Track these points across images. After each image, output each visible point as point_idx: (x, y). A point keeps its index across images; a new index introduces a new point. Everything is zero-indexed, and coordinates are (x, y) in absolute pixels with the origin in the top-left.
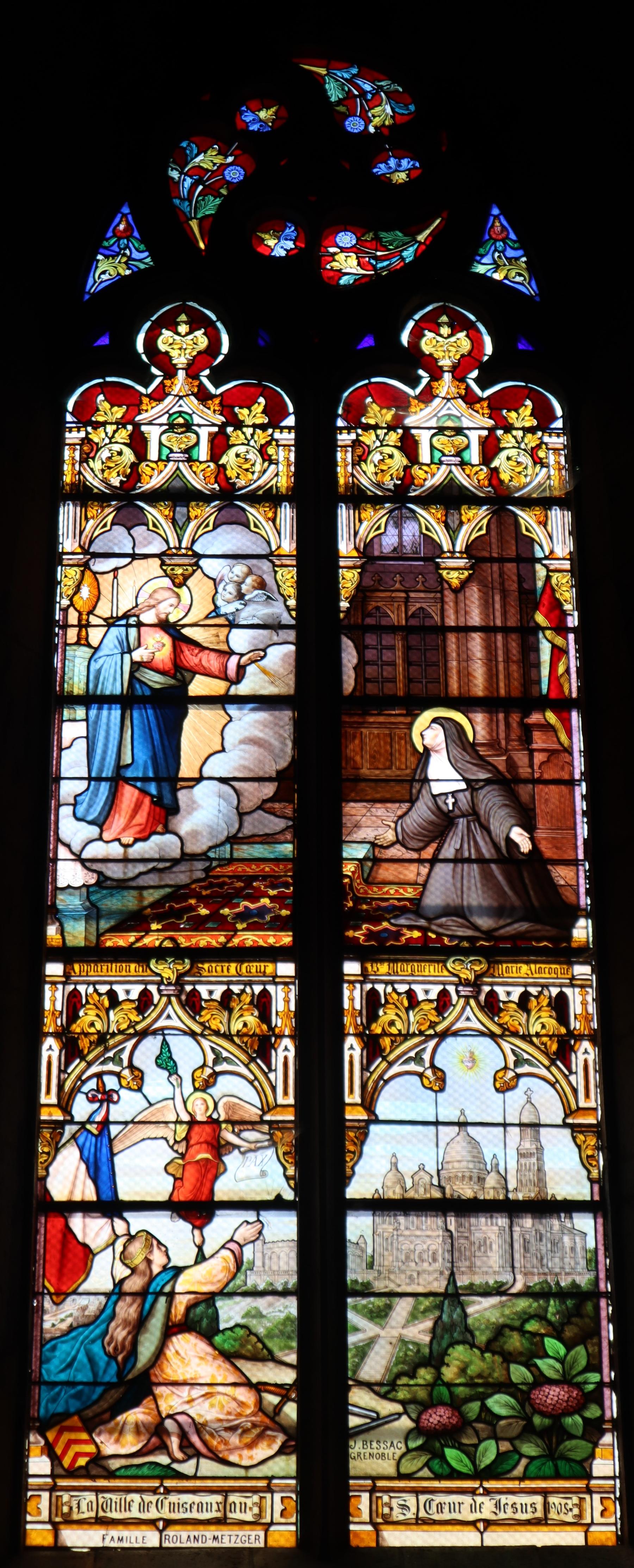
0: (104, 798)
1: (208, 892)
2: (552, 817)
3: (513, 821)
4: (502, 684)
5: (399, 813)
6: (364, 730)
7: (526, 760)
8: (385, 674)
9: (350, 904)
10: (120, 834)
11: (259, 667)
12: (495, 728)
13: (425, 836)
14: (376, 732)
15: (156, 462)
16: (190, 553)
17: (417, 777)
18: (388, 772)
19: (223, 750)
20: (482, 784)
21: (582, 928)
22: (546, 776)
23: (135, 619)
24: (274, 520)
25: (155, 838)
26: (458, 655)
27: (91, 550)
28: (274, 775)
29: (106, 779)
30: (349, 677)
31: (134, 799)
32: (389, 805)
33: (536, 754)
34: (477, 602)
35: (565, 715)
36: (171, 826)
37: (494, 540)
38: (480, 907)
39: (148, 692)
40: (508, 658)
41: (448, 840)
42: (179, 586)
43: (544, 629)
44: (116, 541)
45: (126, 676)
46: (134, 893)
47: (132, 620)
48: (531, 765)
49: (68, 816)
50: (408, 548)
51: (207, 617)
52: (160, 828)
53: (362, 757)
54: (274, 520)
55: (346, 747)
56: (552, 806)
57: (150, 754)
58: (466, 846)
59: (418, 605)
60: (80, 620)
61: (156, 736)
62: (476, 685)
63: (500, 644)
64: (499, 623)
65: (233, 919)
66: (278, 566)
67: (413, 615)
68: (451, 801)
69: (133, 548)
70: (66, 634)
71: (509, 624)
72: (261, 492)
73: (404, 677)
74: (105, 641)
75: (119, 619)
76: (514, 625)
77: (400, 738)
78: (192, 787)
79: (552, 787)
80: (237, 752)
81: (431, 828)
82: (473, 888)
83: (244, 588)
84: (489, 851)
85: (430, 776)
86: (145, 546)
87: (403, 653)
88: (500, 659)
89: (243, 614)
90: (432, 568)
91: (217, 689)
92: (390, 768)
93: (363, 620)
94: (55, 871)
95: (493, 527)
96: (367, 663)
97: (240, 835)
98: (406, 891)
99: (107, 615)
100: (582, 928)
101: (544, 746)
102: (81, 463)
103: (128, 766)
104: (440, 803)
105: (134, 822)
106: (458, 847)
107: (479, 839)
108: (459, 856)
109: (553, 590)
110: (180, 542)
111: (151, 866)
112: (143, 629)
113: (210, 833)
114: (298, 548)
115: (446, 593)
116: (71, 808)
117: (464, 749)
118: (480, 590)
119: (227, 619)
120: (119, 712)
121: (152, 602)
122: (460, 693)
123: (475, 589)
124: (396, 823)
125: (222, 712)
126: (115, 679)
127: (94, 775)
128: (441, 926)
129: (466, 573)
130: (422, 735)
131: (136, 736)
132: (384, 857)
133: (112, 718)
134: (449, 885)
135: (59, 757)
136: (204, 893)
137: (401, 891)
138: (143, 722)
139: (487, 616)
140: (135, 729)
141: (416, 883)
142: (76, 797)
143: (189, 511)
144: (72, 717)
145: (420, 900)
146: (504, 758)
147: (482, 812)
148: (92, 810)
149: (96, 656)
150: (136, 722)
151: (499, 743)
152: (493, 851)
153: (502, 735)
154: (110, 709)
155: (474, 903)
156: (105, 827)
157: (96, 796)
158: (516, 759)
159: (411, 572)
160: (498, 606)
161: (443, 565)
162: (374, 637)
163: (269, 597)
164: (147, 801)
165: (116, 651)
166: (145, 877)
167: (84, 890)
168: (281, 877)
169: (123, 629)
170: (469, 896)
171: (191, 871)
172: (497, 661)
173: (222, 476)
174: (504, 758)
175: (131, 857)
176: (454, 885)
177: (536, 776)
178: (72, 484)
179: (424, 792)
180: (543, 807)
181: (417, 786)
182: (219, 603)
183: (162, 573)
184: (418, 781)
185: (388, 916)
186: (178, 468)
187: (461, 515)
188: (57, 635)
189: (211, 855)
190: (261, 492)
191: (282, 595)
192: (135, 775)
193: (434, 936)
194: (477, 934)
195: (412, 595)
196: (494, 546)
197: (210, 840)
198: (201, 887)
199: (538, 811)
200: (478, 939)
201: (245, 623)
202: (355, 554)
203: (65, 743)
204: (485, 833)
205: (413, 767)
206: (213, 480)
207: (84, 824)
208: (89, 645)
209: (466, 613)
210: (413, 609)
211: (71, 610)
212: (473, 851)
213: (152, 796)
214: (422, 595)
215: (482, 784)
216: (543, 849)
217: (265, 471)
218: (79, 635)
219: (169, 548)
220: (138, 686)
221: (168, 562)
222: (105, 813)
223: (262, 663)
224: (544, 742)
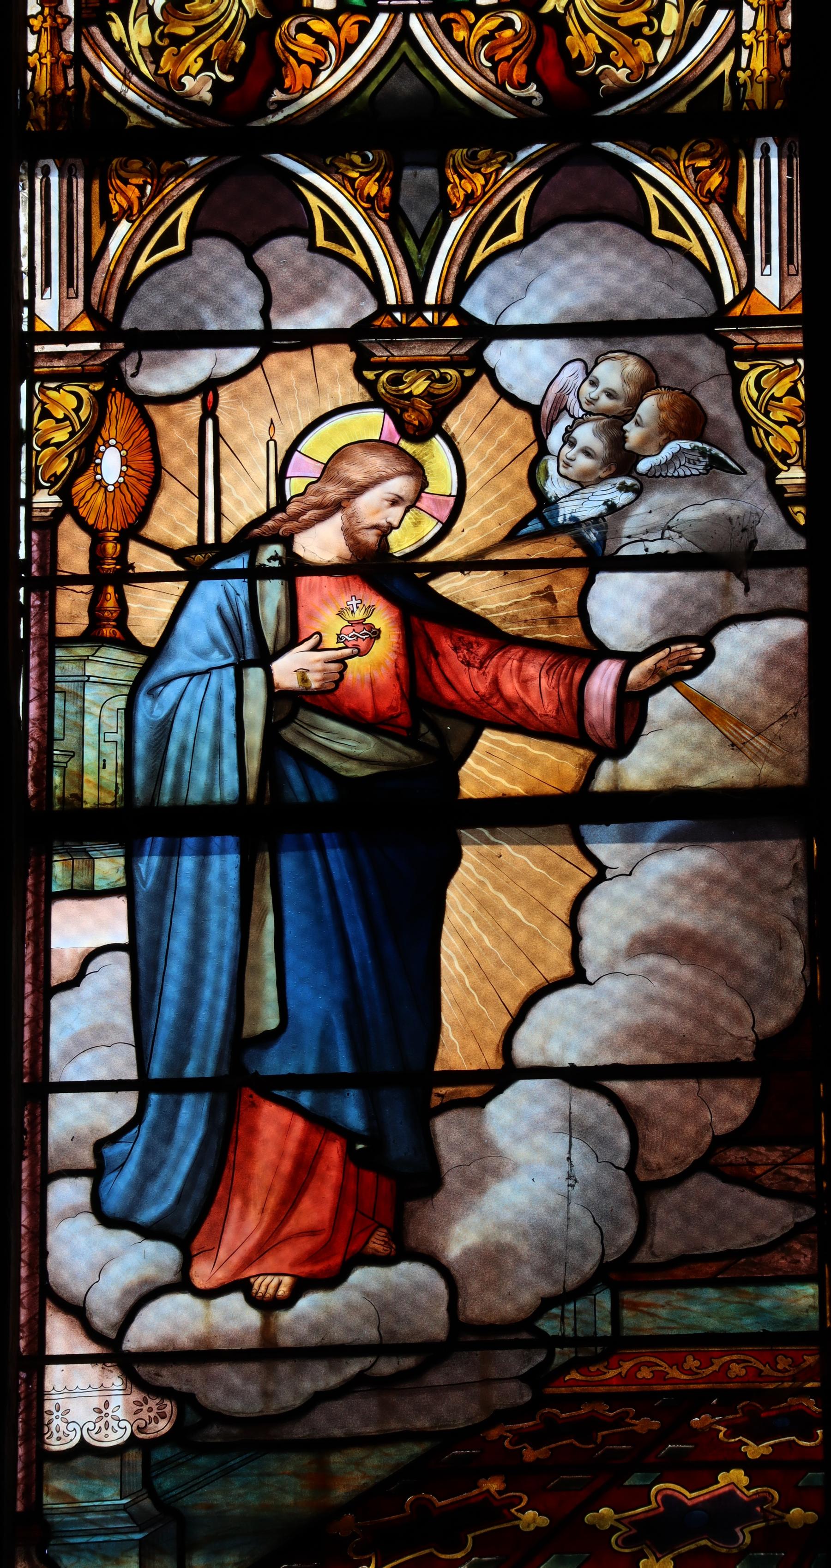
0: (193, 1147)
1: (543, 1452)
10: (248, 1262)
11: (690, 696)
15: (330, 16)
16: (452, 322)
19: (578, 977)
23: (276, 549)
24: (726, 201)
25: (360, 1276)
27: (127, 323)
28: (746, 1054)
29: (197, 1086)
31: (292, 1147)
36: (413, 1240)
39: (324, 791)
42: (421, 436)
44: (205, 287)
45: (254, 738)
46: (299, 1461)
47: (268, 554)
49: (76, 1212)
51: (513, 537)
52: (377, 1244)
54: (726, 201)
57: (338, 991)
60: (96, 556)
61: (356, 929)
65: (627, 1541)
66: (743, 356)
69: (265, 313)
70: (51, 607)
72: (681, 106)
74: (183, 624)
75: (225, 550)
78: (481, 1102)
80: (617, 987)
83: (634, 434)
86: (305, 301)
89: (630, 526)
91: (557, 770)
94: (39, 1394)
97: (643, 1257)
99: (186, 537)
102: (81, 23)
103: (270, 1038)
105: (292, 1226)
110: (419, 287)
111: (353, 1367)
112: (304, 583)
113: (545, 1249)
114: (806, 294)
116: (84, 1184)
119: (580, 542)
120: (233, 859)
121: (333, 492)
125: (571, 851)
126: (217, 751)
127: (156, 1071)
131: (290, 933)
133: (213, 878)
135: (43, 1018)
136: (529, 1455)
138: (311, 883)
140: (289, 911)
142: (99, 1146)
143: (444, 182)
144: (81, 880)
148: (154, 1188)
149: (154, 678)
150: (288, 889)
154: (204, 852)
156: (196, 1244)
157: (168, 1139)
163: (715, 463)
164: (334, 1152)
165: (217, 658)
166: (338, 1406)
167: (134, 1456)
168: (779, 1395)
169: (239, 586)
171: (486, 1381)
173: (550, 52)
175: (286, 1340)
178: (57, 98)
182: (555, 487)
183: (358, 394)
186: (406, 33)
188: (25, 611)
189: (549, 1326)
190: (681, 106)
191: (761, 453)
192: (289, 1068)
197: (543, 1272)
198: (520, 1437)
201: (637, 550)
203: (61, 970)
206: (519, 72)
207: (128, 1236)
208: (130, 643)
211: (67, 524)
213: (349, 1136)
217: (696, 34)
218: (95, 608)
219: (383, 308)
220: (292, 772)
221: (380, 354)
222: (197, 1196)
223: (694, 683)
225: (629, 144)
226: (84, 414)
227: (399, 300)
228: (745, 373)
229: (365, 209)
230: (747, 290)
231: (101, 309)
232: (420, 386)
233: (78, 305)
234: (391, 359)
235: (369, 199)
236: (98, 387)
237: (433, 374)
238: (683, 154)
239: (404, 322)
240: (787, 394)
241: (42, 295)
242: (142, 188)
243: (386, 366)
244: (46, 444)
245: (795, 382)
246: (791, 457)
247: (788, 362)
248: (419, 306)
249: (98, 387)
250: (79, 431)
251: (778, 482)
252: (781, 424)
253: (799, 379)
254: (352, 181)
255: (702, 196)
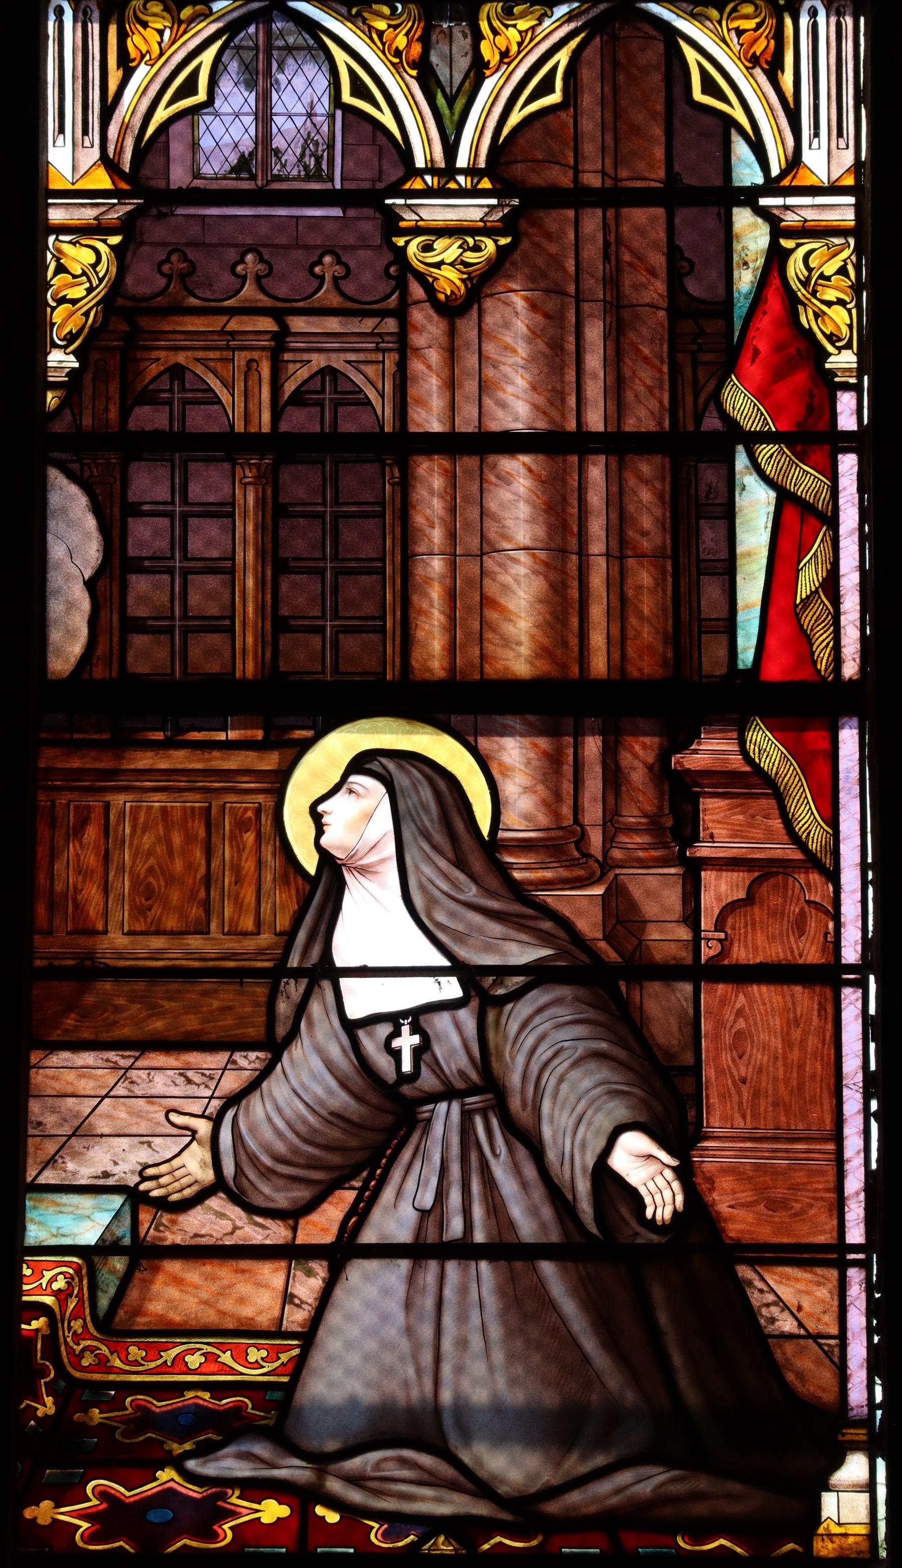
2: (756, 1094)
3: (620, 1111)
4: (598, 639)
5: (231, 1083)
6: (119, 800)
7: (673, 897)
8: (194, 599)
9: (48, 1406)
12: (567, 787)
13: (313, 1164)
14: (157, 801)
17: (294, 961)
18: (195, 942)
20: (518, 981)
21: (857, 1488)
22: (740, 954)
24: (773, 70)
26: (452, 536)
30: (71, 606)
32: (194, 1058)
33: (707, 876)
34: (522, 350)
35: (816, 738)
37: (588, 125)
38: (497, 1409)
40: (623, 542)
41: (397, 1174)
43: (752, 440)
48: (691, 917)
50: (290, 157)
53: (106, 890)
54: (773, 70)
55: (53, 855)
56: (760, 1057)
58: (455, 1197)
59: (318, 361)
62: (507, 642)
63: (596, 498)
64: (595, 421)
67: (299, 398)
68: (407, 1042)
71: (631, 425)
73: (261, 609)
76: (650, 425)
77: (241, 825)
79: (761, 992)
81: (335, 1134)
82: (476, 1342)
84: (533, 1211)
85: (341, 959)
87: (261, 528)
88: (597, 547)
90: (370, 227)
92: (203, 930)
93: (125, 414)
95: (587, 75)
96: (136, 566)
98: (241, 1356)
100: (857, 1488)
101: (738, 848)
104: (371, 1044)
106: (427, 1199)
107: (500, 1171)
108: (431, 1236)
109: (792, 301)
110: (451, 150)
115: (417, 315)
117: (460, 863)
118: (533, 306)
122: (452, 668)
123: (519, 302)
124: (217, 1121)
128: (356, 1480)
129: (489, 246)
130: (317, 818)
132: (173, 1238)
134: (392, 1332)
137: (226, 1358)
139: (557, 397)
141: (278, 1332)
145: (290, 1388)
146: (598, 891)
147: (515, 1079)
151: (582, 839)
152: (547, 1212)
153: (593, 813)
155: (480, 1396)
158: (636, 892)
159: (297, 245)
160: (594, 361)
161: (409, 219)
162: (163, 471)
170: (459, 1370)
172: (582, 552)
174: (598, 891)
176: (409, 1331)
177: (707, 952)
179: (315, 1008)
180: (726, 1058)
181: (294, 989)
184: (297, 973)
185: (177, 1449)
187: (478, 37)
193: (332, 1517)
194: (481, 1509)
195: (298, 324)
196: (589, 148)
199: (708, 1072)
200: (489, 1527)
202: (102, 181)
204: (522, 1152)
205: (283, 922)
209: (484, 387)
210: (304, 373)
212: (478, 1212)
214: (333, 324)
215: (518, 981)
216: (723, 1208)
224: (735, 835)
225: (323, 5)
226: (102, 269)
227: (471, 163)
228: (792, 251)
229: (393, 64)
230: (794, 162)
231: (116, 158)
232: (453, 253)
233: (95, 154)
234: (420, 223)
235: (398, 53)
236: (115, 240)
237: (466, 241)
238: (725, 16)
239: (469, 186)
240: (836, 274)
241: (54, 142)
242: (161, 32)
243: (416, 231)
244: (62, 301)
245: (845, 261)
246: (840, 340)
247: (836, 241)
248: (450, 171)
249: (115, 240)
250: (98, 286)
251: (827, 366)
252: (829, 304)
253: (849, 257)
254: (381, 34)
255: (746, 59)
